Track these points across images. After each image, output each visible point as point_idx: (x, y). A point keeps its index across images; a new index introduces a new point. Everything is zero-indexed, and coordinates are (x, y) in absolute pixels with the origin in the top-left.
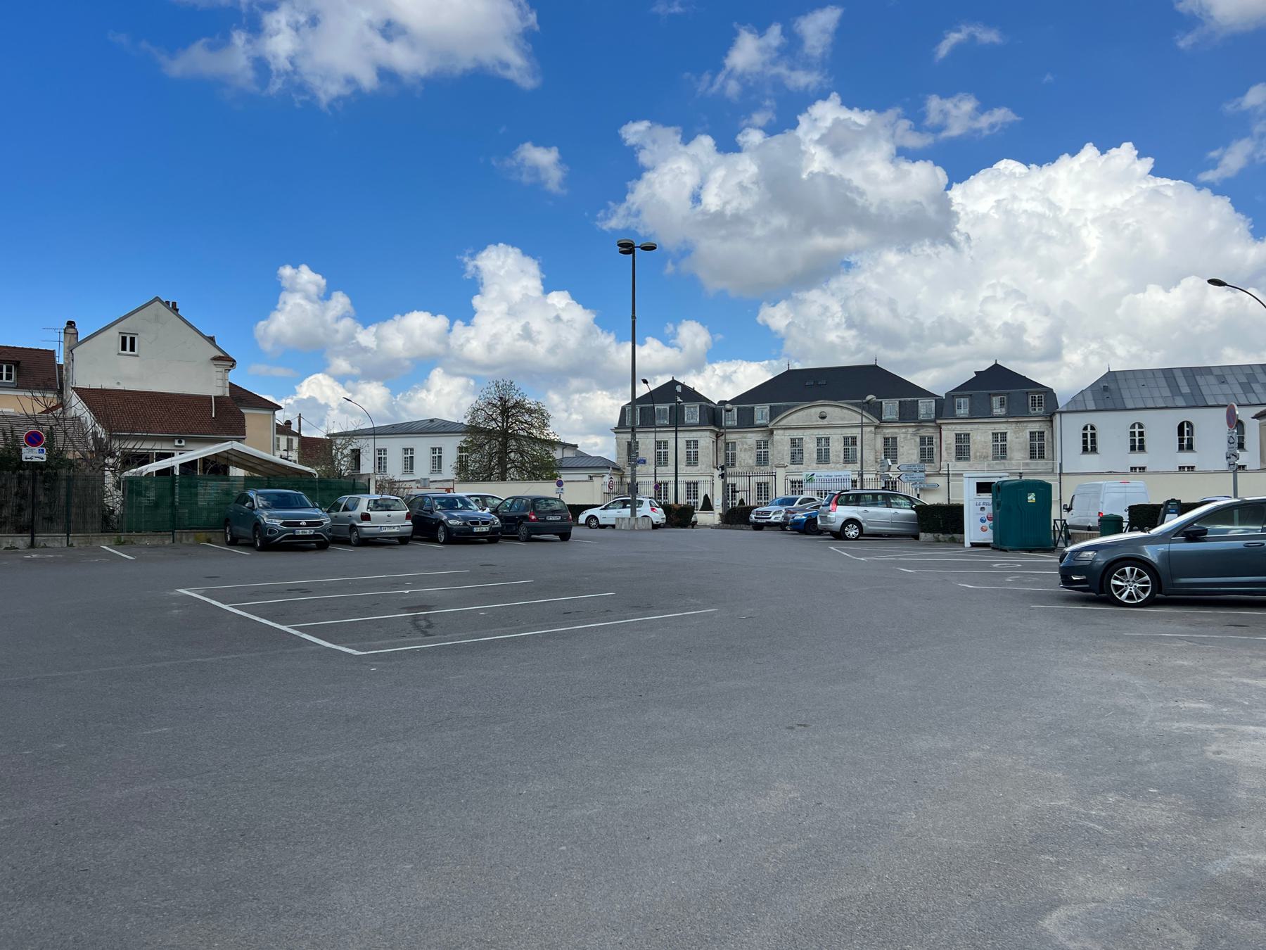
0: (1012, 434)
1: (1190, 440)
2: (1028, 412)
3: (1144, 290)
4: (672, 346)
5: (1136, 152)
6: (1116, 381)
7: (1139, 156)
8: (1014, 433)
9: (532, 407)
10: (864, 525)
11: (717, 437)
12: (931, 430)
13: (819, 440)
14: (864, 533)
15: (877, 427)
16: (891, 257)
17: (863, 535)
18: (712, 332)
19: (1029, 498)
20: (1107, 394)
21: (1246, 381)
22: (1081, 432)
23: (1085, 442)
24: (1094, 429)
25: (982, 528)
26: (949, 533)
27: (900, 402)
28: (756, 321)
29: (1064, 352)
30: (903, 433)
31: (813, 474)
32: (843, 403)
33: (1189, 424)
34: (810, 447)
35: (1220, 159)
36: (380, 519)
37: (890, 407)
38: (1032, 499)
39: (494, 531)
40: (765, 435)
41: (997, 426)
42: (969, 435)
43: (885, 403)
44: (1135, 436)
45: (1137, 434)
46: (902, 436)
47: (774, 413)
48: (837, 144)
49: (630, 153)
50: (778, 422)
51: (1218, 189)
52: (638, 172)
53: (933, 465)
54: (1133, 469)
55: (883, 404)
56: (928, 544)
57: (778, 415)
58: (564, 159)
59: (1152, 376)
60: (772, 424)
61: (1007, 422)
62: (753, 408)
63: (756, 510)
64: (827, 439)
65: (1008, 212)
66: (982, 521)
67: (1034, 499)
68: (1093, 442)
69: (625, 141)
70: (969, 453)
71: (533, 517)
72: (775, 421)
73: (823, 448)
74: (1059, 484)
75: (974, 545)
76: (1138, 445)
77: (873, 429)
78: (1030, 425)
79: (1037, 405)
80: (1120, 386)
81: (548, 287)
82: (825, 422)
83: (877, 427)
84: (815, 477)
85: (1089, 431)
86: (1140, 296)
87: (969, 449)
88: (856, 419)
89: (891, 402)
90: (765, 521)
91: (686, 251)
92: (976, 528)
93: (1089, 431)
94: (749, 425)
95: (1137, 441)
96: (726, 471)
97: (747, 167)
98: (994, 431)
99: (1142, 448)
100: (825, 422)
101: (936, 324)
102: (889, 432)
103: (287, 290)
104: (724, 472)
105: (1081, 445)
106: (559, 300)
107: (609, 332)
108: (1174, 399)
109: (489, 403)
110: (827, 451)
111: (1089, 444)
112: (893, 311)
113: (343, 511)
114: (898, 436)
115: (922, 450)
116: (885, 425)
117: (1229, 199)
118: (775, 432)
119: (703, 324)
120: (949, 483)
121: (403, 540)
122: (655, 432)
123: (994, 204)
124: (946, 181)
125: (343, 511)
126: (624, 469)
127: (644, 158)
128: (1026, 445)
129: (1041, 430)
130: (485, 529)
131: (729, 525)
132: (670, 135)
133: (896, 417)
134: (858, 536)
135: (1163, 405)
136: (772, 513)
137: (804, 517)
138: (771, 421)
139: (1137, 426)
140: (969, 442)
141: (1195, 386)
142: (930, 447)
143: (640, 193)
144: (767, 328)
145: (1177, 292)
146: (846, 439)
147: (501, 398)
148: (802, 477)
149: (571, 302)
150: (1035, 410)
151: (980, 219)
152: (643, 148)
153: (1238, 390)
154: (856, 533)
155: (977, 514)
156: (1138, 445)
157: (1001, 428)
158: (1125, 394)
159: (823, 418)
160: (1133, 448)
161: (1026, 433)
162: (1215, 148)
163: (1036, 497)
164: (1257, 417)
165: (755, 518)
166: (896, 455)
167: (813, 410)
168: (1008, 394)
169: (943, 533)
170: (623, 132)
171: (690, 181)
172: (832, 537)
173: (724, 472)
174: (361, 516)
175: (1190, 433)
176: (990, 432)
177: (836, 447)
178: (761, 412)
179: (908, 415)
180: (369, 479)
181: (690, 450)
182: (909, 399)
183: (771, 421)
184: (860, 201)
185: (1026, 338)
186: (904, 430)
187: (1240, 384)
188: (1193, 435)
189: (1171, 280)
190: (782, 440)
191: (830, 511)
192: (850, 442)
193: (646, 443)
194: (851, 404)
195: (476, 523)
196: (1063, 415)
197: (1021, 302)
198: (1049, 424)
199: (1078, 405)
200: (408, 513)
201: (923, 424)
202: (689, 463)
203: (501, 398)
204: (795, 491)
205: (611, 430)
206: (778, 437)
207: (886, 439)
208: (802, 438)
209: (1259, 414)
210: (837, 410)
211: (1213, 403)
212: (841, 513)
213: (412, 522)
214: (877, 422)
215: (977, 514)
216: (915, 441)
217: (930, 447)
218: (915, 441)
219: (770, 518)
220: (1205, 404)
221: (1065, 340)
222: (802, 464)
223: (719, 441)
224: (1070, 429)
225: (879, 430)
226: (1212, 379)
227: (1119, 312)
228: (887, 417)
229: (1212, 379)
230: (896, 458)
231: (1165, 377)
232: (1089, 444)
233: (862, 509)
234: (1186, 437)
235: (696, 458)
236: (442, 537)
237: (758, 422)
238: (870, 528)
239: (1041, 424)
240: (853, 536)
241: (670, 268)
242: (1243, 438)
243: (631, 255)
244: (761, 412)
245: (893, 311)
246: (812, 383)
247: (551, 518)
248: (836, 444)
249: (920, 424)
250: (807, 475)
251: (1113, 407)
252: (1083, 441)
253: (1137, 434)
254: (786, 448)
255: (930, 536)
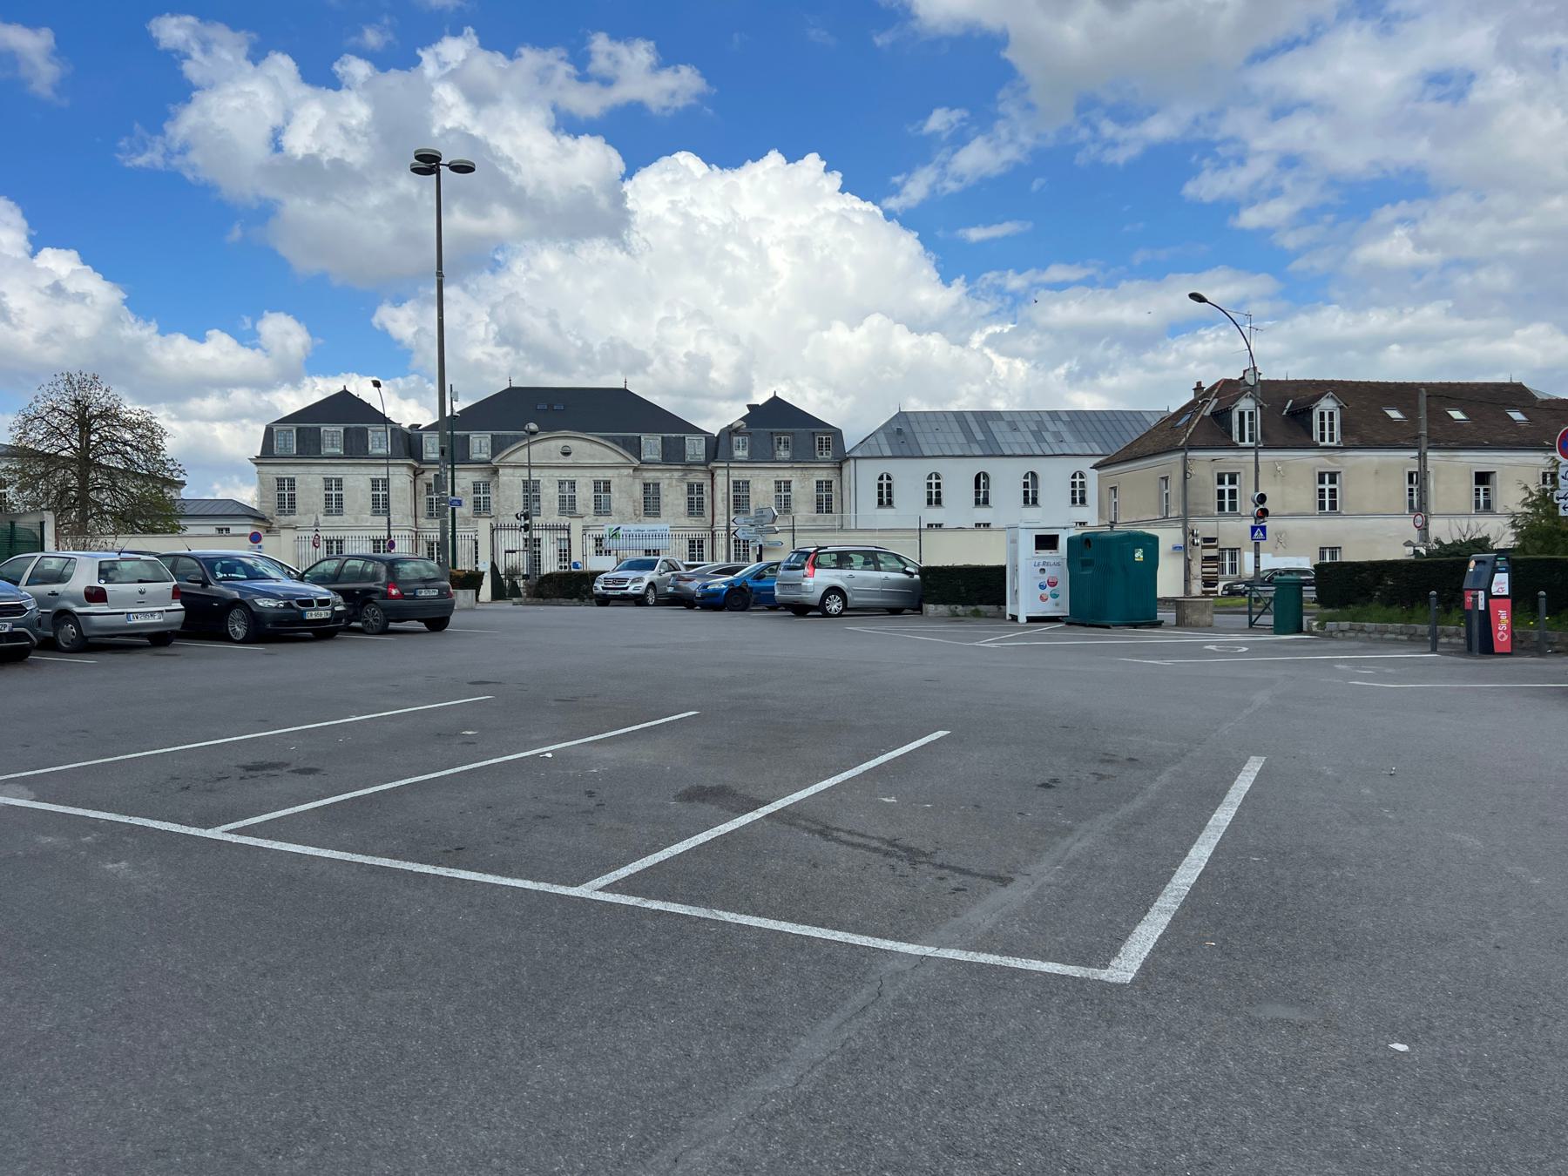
0: (798, 483)
1: (986, 493)
2: (815, 457)
3: (829, 328)
4: (253, 347)
5: (824, 163)
6: (909, 422)
7: (827, 170)
8: (800, 481)
9: (134, 417)
10: (849, 595)
11: (415, 475)
12: (701, 475)
13: (561, 483)
14: (848, 606)
15: (636, 469)
16: (549, 259)
17: (848, 610)
18: (311, 331)
19: (1137, 555)
20: (901, 439)
21: (1036, 429)
22: (877, 482)
23: (880, 494)
24: (890, 479)
25: (1041, 597)
26: (972, 605)
27: (663, 438)
28: (371, 324)
29: (754, 392)
30: (667, 478)
31: (619, 528)
32: (593, 436)
33: (986, 476)
34: (585, 494)
35: (903, 184)
36: (125, 600)
37: (652, 444)
38: (1139, 557)
39: (337, 616)
40: (485, 474)
41: (780, 473)
42: (748, 482)
43: (644, 438)
44: (931, 488)
45: (934, 486)
46: (667, 481)
47: (498, 446)
48: (478, 97)
49: (172, 60)
50: (503, 458)
51: (907, 220)
52: (185, 92)
53: (703, 519)
54: (978, 525)
55: (642, 439)
56: (939, 618)
57: (507, 448)
58: (62, 49)
59: (944, 419)
60: (497, 459)
61: (792, 468)
62: (468, 436)
63: (602, 576)
64: (573, 484)
65: (686, 216)
66: (1042, 587)
67: (1142, 557)
68: (889, 494)
69: (157, 41)
70: (749, 504)
71: (394, 592)
72: (500, 456)
73: (567, 495)
74: (918, 542)
75: (1030, 619)
76: (935, 500)
77: (631, 471)
78: (817, 472)
79: (824, 448)
80: (914, 429)
81: (36, 245)
82: (569, 460)
83: (636, 469)
84: (621, 532)
85: (885, 482)
86: (826, 335)
87: (748, 501)
88: (614, 458)
89: (651, 437)
90: (619, 592)
91: (265, 212)
92: (1025, 598)
93: (885, 482)
94: (463, 460)
95: (934, 494)
96: (531, 522)
97: (356, 110)
98: (778, 479)
99: (938, 502)
100: (569, 460)
101: (608, 347)
102: (650, 476)
103: (198, 89)
104: (527, 522)
105: (877, 498)
106: (59, 263)
107: (147, 320)
108: (970, 447)
109: (54, 409)
110: (573, 499)
111: (885, 498)
112: (555, 326)
113: (27, 585)
114: (661, 481)
115: (691, 501)
116: (645, 466)
117: (917, 234)
118: (501, 471)
119: (299, 319)
120: (794, 540)
121: (159, 639)
122: (388, 465)
123: (669, 206)
124: (623, 170)
125: (27, 585)
126: (272, 518)
127: (191, 70)
128: (812, 496)
129: (829, 479)
130: (324, 614)
131: (541, 600)
132: (229, 48)
133: (657, 457)
134: (842, 611)
135: (961, 453)
136: (629, 581)
137: (724, 586)
138: (493, 456)
139: (934, 476)
140: (748, 491)
141: (988, 432)
142: (699, 496)
143: (188, 121)
144: (385, 333)
145: (861, 331)
146: (597, 483)
147: (77, 402)
148: (605, 532)
149: (81, 267)
150: (822, 454)
151: (655, 222)
152: (188, 57)
153: (1031, 439)
154: (839, 607)
155: (1036, 578)
156: (935, 500)
157: (785, 475)
158: (921, 440)
159: (567, 454)
160: (929, 502)
161: (812, 482)
162: (898, 173)
163: (1144, 554)
164: (1096, 467)
165: (603, 588)
166: (659, 506)
167: (553, 443)
168: (793, 434)
169: (963, 605)
170: (153, 28)
171: (272, 117)
172: (790, 613)
173: (527, 522)
174: (86, 593)
175: (987, 486)
176: (773, 480)
177: (585, 494)
178: (480, 444)
179: (673, 455)
180: (42, 524)
181: (330, 492)
182: (674, 435)
183: (493, 456)
184: (517, 180)
185: (714, 375)
186: (668, 475)
187: (1031, 431)
188: (988, 488)
189: (855, 318)
190: (511, 482)
191: (805, 576)
192: (603, 487)
193: (310, 480)
194: (601, 437)
195: (309, 603)
196: (858, 461)
197: (704, 327)
198: (838, 472)
199: (870, 449)
200: (175, 586)
201: (692, 467)
202: (328, 511)
203: (77, 402)
204: (601, 552)
205: (250, 459)
206: (505, 478)
207: (646, 486)
208: (539, 481)
209: (1097, 464)
210: (584, 444)
211: (1009, 453)
212: (817, 581)
213: (182, 603)
214: (636, 463)
215: (1036, 578)
216: (682, 489)
217: (699, 496)
218: (682, 489)
219: (627, 588)
220: (1001, 453)
221: (755, 376)
222: (540, 515)
223: (418, 482)
224: (865, 476)
225: (637, 473)
226: (1003, 426)
227: (806, 352)
228: (647, 457)
229: (1003, 426)
230: (659, 510)
231: (977, 421)
232: (885, 498)
233: (846, 573)
234: (982, 490)
235: (340, 503)
236: (239, 630)
237: (474, 456)
238: (856, 599)
239: (829, 471)
240: (836, 611)
241: (236, 233)
242: (1036, 491)
243: (435, 175)
244: (480, 444)
245: (555, 326)
246: (546, 408)
247: (424, 593)
248: (585, 489)
249: (689, 467)
250: (610, 530)
251: (910, 454)
252: (879, 492)
253: (934, 486)
254: (516, 494)
255: (942, 609)
